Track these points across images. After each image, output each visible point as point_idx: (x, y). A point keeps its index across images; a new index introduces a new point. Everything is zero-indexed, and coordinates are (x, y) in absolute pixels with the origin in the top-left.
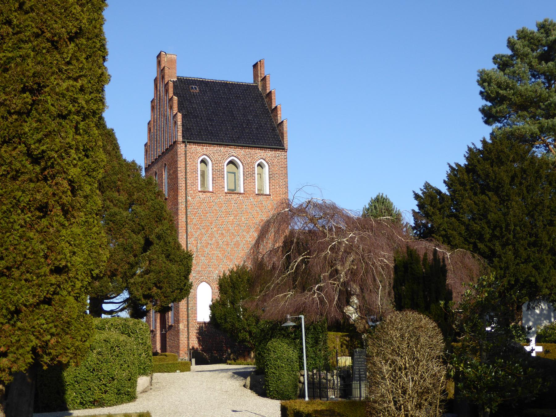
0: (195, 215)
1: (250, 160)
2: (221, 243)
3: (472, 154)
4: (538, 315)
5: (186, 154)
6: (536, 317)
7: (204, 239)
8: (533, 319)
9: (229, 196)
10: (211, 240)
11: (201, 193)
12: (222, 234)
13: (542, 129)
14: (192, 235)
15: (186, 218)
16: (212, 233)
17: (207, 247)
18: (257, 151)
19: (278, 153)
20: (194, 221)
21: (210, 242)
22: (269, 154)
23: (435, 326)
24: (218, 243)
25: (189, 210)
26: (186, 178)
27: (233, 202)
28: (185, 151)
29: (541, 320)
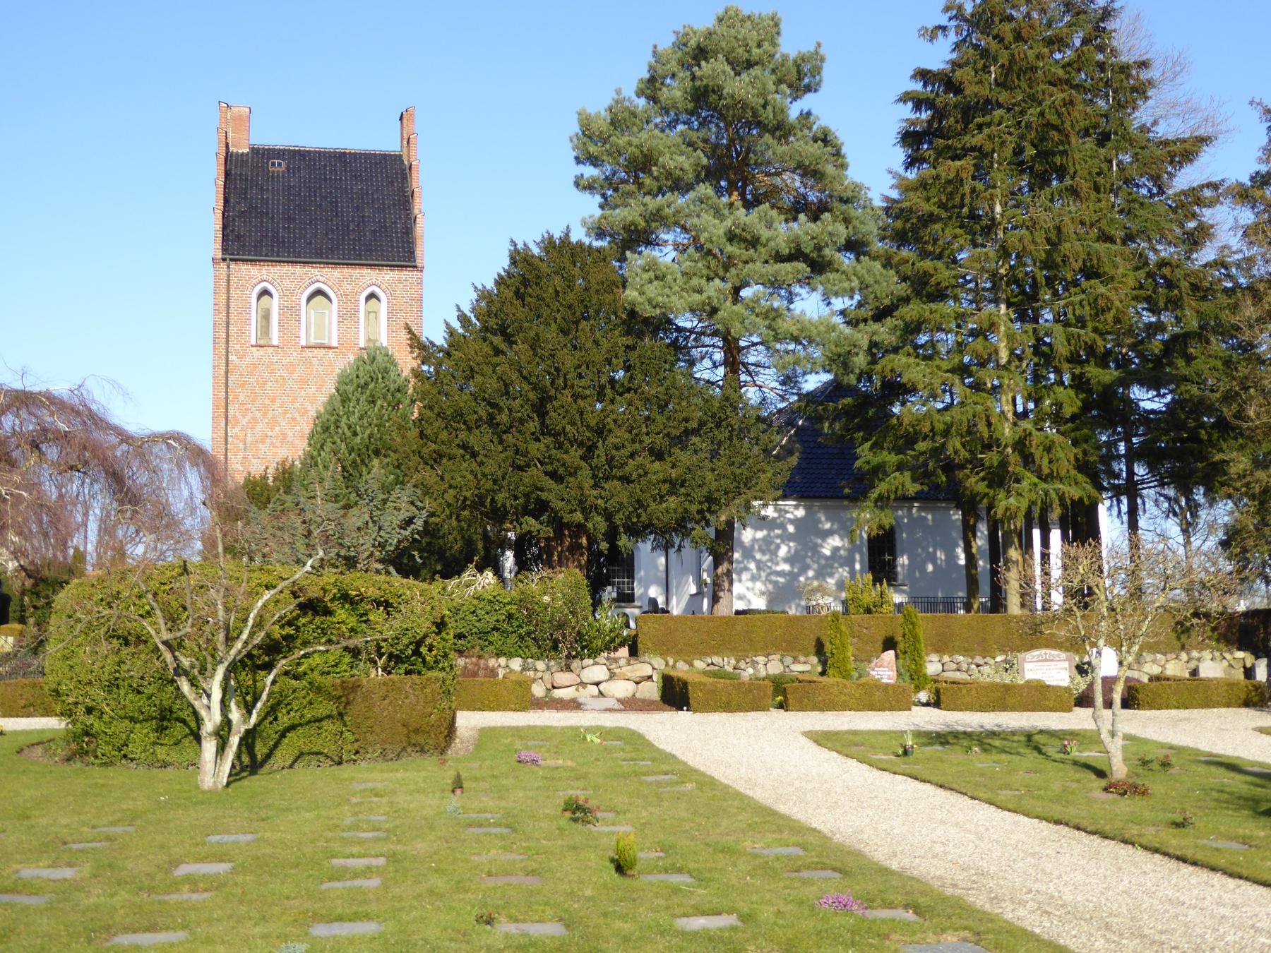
0: (242, 386)
1: (350, 287)
2: (290, 434)
3: (549, 244)
4: (827, 558)
5: (228, 281)
6: (823, 562)
7: (257, 431)
8: (815, 566)
9: (307, 353)
10: (272, 429)
11: (254, 349)
12: (294, 419)
13: (1254, 297)
14: (237, 422)
15: (227, 393)
16: (273, 418)
17: (263, 442)
18: (365, 271)
19: (405, 274)
20: (241, 398)
21: (270, 434)
22: (387, 277)
23: (807, 531)
24: (284, 435)
25: (231, 378)
26: (228, 323)
27: (315, 361)
28: (229, 276)
29: (832, 567)
